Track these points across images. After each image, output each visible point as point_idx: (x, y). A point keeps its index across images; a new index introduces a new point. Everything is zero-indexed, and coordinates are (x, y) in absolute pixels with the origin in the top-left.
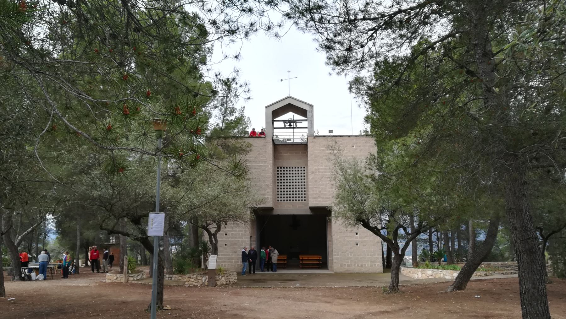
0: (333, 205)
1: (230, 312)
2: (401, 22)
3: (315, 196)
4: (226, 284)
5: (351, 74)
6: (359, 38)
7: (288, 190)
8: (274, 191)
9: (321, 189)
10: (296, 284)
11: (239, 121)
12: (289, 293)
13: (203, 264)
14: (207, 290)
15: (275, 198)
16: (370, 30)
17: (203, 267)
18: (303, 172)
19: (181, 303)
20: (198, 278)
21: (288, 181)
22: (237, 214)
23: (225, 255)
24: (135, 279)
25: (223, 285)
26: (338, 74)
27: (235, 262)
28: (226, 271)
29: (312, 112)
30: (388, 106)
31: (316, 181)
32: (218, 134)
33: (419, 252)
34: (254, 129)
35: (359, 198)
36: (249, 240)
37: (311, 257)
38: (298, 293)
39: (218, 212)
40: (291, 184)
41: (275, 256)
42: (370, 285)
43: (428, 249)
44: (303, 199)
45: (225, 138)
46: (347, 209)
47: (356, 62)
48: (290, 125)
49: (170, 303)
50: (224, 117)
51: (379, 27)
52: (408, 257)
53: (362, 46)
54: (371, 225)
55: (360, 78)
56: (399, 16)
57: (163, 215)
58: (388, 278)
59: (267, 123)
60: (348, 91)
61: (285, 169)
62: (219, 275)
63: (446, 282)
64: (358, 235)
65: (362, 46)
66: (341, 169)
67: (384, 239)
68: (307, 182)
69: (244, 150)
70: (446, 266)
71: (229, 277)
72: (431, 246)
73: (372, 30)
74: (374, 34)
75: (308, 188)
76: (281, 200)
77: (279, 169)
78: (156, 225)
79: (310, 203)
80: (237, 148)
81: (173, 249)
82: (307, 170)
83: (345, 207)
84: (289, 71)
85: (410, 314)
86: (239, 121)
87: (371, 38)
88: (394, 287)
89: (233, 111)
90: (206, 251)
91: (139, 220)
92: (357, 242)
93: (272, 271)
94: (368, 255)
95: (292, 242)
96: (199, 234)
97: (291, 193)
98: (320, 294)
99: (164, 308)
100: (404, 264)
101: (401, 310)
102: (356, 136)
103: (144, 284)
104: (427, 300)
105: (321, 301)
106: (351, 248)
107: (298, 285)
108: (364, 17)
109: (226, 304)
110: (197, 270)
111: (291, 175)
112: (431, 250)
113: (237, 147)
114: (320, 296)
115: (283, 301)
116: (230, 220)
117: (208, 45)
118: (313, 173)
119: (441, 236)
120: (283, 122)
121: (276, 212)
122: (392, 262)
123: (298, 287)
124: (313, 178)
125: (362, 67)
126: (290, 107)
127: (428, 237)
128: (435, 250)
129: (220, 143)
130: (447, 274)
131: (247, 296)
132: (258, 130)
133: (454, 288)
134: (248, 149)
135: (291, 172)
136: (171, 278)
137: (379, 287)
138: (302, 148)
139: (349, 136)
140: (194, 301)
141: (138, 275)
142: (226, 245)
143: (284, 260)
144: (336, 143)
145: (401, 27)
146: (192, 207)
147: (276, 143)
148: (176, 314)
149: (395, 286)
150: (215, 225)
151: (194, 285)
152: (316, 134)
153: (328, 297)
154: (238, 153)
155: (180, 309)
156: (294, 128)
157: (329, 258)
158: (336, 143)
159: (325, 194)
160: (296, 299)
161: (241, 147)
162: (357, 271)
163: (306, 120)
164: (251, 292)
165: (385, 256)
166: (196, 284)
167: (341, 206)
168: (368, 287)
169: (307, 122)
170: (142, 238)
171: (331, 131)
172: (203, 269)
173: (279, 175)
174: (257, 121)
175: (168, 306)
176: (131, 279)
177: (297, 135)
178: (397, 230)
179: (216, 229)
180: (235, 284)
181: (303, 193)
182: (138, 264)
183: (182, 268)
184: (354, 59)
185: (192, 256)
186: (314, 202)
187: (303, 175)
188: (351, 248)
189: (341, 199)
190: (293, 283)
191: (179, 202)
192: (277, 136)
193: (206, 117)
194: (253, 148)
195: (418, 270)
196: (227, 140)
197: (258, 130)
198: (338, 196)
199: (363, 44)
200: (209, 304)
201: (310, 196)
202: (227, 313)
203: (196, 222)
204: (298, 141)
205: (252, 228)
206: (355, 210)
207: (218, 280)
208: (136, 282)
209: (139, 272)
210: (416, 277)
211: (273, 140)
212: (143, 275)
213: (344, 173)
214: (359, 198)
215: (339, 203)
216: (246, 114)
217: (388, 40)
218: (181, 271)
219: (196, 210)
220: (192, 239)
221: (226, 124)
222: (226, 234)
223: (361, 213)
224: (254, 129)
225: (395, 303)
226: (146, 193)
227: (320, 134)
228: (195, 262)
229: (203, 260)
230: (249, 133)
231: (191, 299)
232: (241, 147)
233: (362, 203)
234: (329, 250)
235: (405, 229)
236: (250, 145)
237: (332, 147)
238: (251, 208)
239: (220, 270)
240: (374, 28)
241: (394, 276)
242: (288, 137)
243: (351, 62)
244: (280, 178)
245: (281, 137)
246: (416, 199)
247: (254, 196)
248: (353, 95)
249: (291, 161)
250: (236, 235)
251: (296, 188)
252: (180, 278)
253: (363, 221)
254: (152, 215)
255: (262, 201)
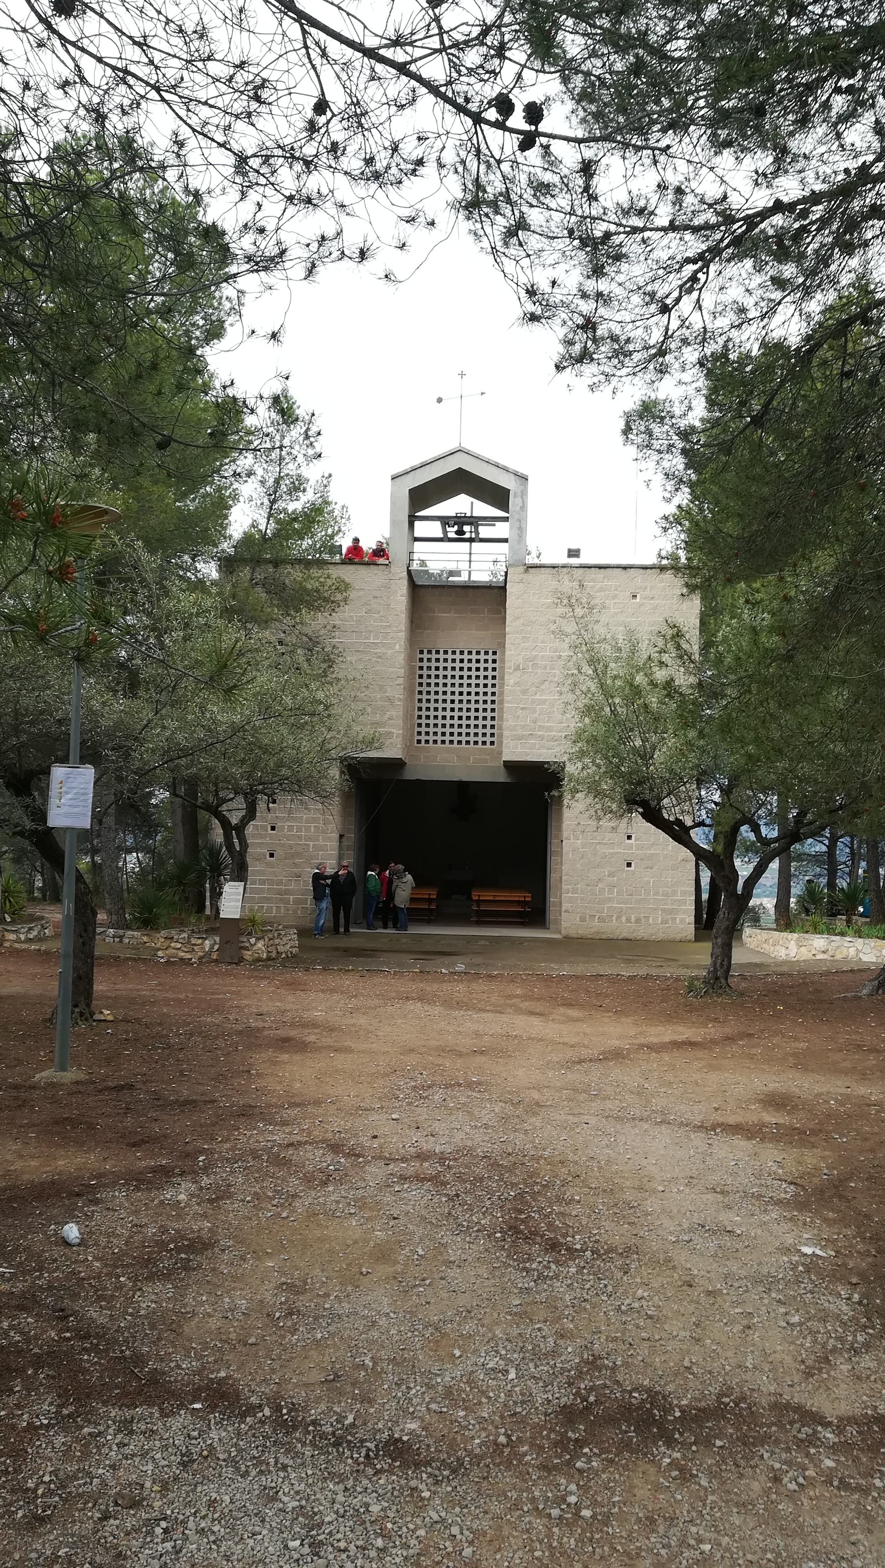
0: (565, 758)
1: (272, 1033)
2: (780, 236)
3: (520, 732)
4: (269, 959)
5: (632, 391)
6: (656, 286)
7: (448, 714)
8: (408, 716)
9: (537, 717)
10: (455, 964)
11: (315, 514)
12: (435, 986)
13: (208, 903)
14: (216, 974)
15: (412, 735)
16: (688, 261)
17: (208, 912)
18: (490, 665)
19: (143, 1004)
20: (193, 941)
21: (449, 689)
22: (301, 776)
23: (271, 882)
24: (23, 937)
25: (259, 960)
26: (592, 388)
27: (296, 902)
28: (271, 924)
29: (524, 494)
30: (724, 489)
31: (525, 692)
32: (253, 551)
33: (797, 889)
34: (356, 540)
35: (638, 743)
36: (336, 844)
37: (502, 896)
38: (461, 987)
39: (245, 768)
40: (457, 698)
41: (405, 888)
42: (654, 972)
43: (824, 881)
44: (488, 739)
45: (276, 563)
46: (603, 769)
47: (645, 355)
48: (460, 532)
49: (113, 1002)
50: (273, 502)
51: (715, 251)
52: (764, 900)
53: (665, 309)
54: (666, 816)
55: (655, 403)
56: (778, 220)
57: (88, 773)
58: (703, 955)
59: (394, 523)
60: (621, 439)
61: (442, 656)
62: (250, 934)
63: (858, 972)
64: (632, 841)
65: (665, 309)
66: (592, 662)
67: (700, 854)
68: (502, 693)
69: (326, 600)
70: (865, 929)
71: (277, 941)
72: (832, 874)
73: (694, 261)
74: (700, 275)
75: (502, 710)
76: (435, 742)
77: (425, 656)
78: (71, 796)
79: (505, 750)
80: (308, 592)
81: (132, 861)
82: (503, 661)
83: (598, 766)
84: (462, 375)
85: (754, 1051)
86: (315, 514)
87: (691, 284)
88: (717, 978)
89: (297, 486)
90: (216, 873)
91: (29, 784)
92: (629, 859)
93: (395, 927)
94: (657, 894)
95: (454, 854)
96: (200, 826)
97: (456, 722)
98: (519, 991)
99: (95, 1017)
100: (756, 921)
101: (729, 1039)
102: (645, 568)
103: (47, 953)
104: (801, 1016)
105: (519, 1011)
106: (611, 874)
107: (460, 967)
108: (672, 222)
109: (264, 1009)
110: (193, 920)
111: (457, 673)
112: (831, 885)
113: (305, 589)
114: (517, 996)
115: (416, 1007)
116: (284, 790)
117: (228, 290)
118: (517, 668)
119: (860, 847)
120: (438, 524)
121: (410, 775)
122: (721, 911)
123: (460, 973)
124: (517, 684)
125: (662, 371)
126: (460, 481)
127: (824, 849)
128: (842, 883)
129: (259, 576)
130: (867, 949)
131: (323, 991)
132: (368, 545)
133: (879, 988)
134: (339, 597)
135: (458, 665)
136: (121, 937)
137: (677, 979)
138: (491, 597)
139: (625, 568)
140: (179, 1001)
141: (30, 929)
142: (272, 855)
143: (430, 901)
144: (582, 586)
145: (782, 255)
146: (172, 754)
147: (419, 582)
148: (127, 1032)
149: (720, 976)
150: (240, 803)
151: (182, 959)
152: (531, 560)
153: (539, 999)
154: (310, 606)
155: (138, 1021)
156: (471, 540)
157: (552, 899)
158: (582, 586)
159: (549, 729)
160: (450, 1003)
161: (318, 591)
162: (625, 935)
163: (506, 519)
164: (333, 980)
165: (705, 896)
166: (188, 956)
167: (587, 760)
168: (646, 978)
169: (506, 524)
170: (34, 832)
171: (573, 553)
172: (208, 918)
173: (425, 672)
174: (366, 517)
175: (107, 1012)
176: (12, 937)
177: (479, 564)
178: (735, 830)
179: (243, 813)
180: (291, 961)
181: (489, 723)
182: (34, 899)
183: (150, 912)
184: (638, 346)
185: (180, 883)
186: (516, 750)
187: (490, 673)
188: (611, 874)
189: (590, 743)
190: (447, 960)
191: (136, 739)
192: (423, 563)
193: (220, 506)
194: (353, 595)
195: (790, 936)
196: (281, 569)
197: (368, 545)
198: (578, 737)
199: (668, 301)
200: (219, 1008)
201: (506, 733)
202: (265, 1033)
203: (192, 792)
204: (481, 576)
205: (345, 813)
206: (622, 775)
207: (247, 949)
208: (25, 946)
209: (32, 919)
210: (781, 953)
211: (409, 572)
212: (43, 928)
213: (599, 677)
214: (638, 743)
215: (582, 754)
216: (335, 495)
217: (735, 293)
218: (148, 922)
219: (183, 761)
220: (180, 837)
221: (278, 522)
222: (273, 828)
223: (640, 783)
224: (356, 540)
225: (716, 1020)
226: (42, 713)
227: (544, 560)
228: (187, 899)
229: (208, 894)
230: (344, 551)
231: (170, 995)
232: (318, 591)
233: (646, 756)
234: (552, 877)
235: (756, 829)
236: (343, 586)
237: (569, 598)
238: (342, 760)
239: (253, 921)
240: (701, 257)
241: (718, 951)
242: (452, 566)
243: (630, 353)
244: (425, 680)
245: (435, 566)
246: (780, 751)
247: (349, 727)
248: (632, 451)
249: (461, 635)
250: (299, 829)
251: (468, 710)
252: (145, 939)
253: (644, 804)
254: (58, 772)
255: (370, 743)
